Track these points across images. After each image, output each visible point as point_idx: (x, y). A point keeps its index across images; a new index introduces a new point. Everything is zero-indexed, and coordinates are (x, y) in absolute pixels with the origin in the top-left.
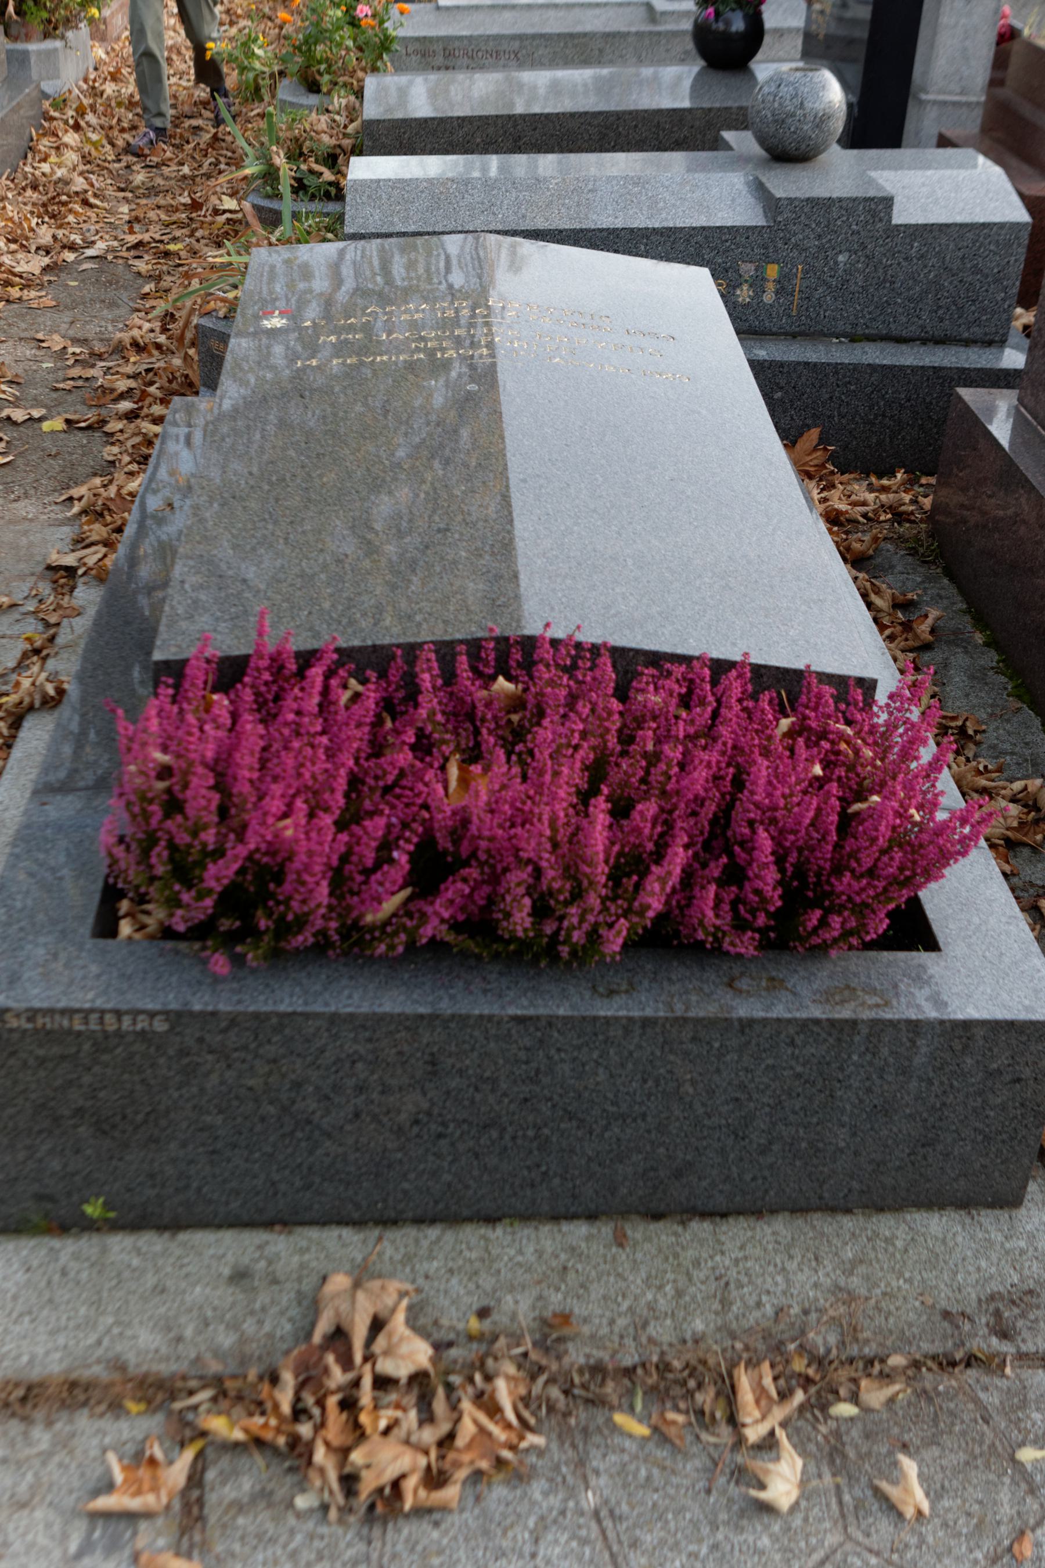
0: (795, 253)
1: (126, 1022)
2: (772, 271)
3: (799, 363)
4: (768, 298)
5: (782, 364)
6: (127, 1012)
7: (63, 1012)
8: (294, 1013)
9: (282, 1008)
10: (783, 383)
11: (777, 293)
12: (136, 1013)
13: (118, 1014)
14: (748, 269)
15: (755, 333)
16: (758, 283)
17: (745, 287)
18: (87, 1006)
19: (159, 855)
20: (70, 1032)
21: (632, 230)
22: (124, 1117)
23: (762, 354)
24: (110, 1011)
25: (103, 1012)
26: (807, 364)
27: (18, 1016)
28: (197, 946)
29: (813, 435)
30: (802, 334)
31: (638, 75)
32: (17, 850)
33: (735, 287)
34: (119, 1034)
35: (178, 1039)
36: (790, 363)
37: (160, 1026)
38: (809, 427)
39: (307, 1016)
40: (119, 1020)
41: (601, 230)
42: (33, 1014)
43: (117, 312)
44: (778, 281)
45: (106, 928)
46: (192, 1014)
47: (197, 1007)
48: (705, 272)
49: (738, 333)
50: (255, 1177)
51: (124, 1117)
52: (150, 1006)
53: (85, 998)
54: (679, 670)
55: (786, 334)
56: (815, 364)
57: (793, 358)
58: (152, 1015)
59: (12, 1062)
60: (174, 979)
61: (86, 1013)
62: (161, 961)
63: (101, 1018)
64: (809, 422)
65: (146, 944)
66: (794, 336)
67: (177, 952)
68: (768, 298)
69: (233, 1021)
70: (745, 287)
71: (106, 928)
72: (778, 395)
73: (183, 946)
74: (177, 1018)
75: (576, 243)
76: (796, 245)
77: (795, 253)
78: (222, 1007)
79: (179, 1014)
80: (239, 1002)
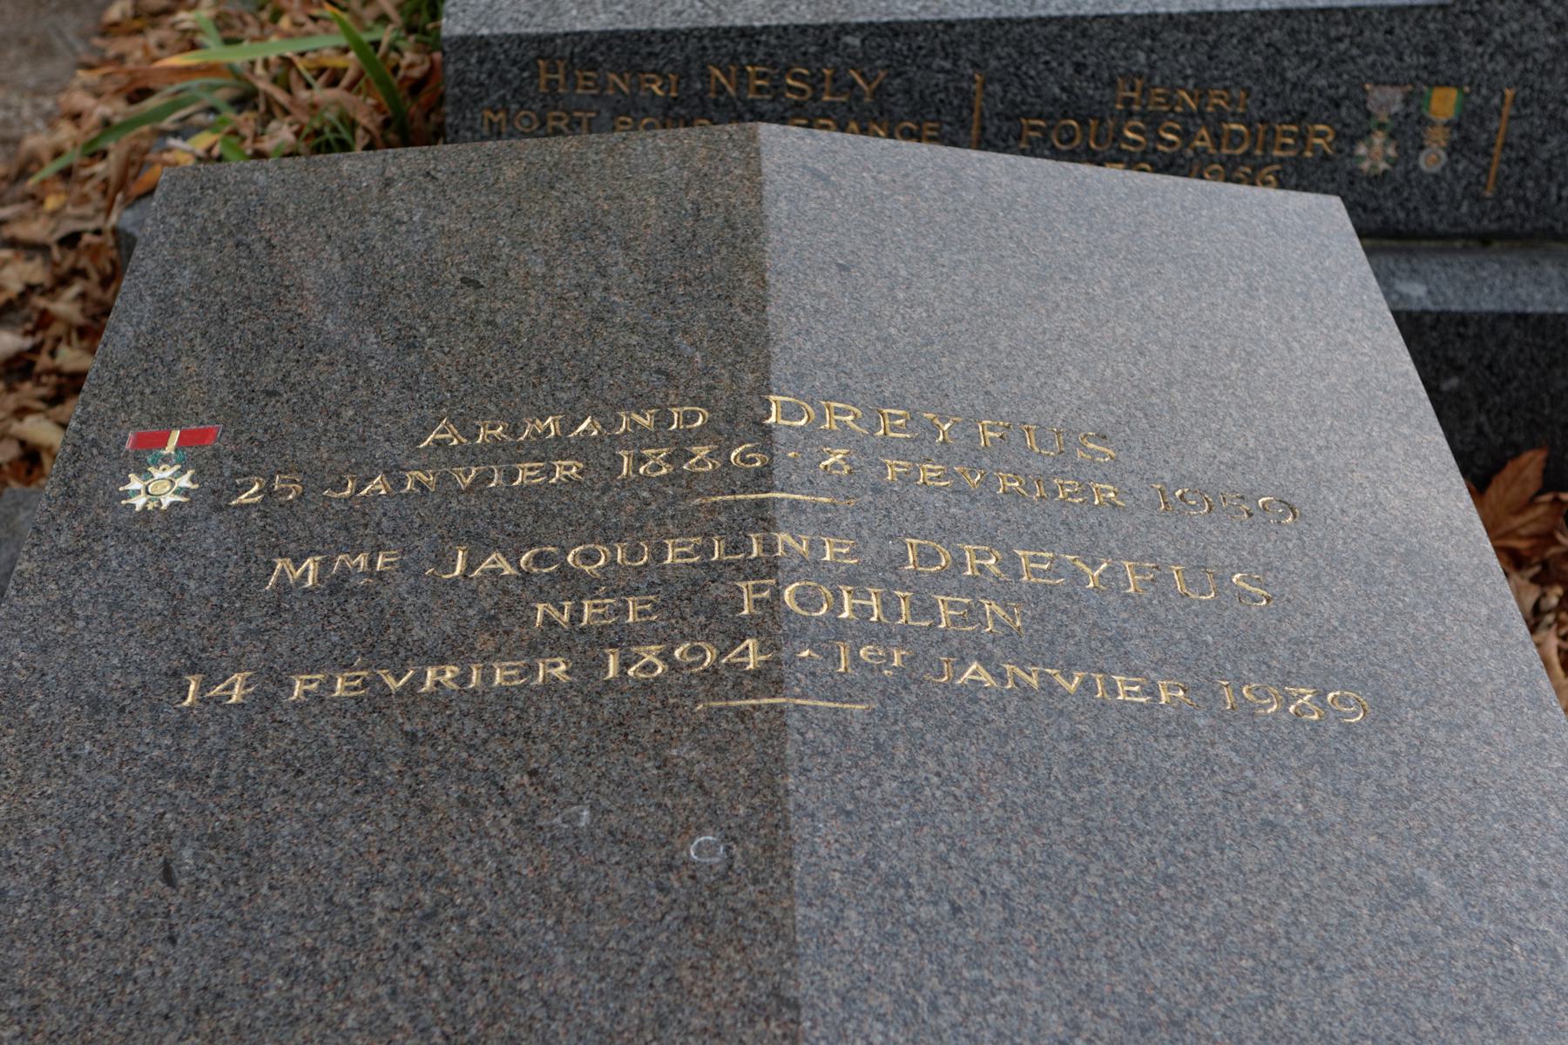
0: (1501, 63)
2: (1444, 104)
3: (1503, 316)
4: (1432, 160)
5: (1462, 319)
10: (1462, 357)
11: (1452, 149)
14: (1386, 100)
15: (1397, 235)
16: (1408, 130)
17: (1378, 139)
21: (1117, 20)
23: (1416, 292)
26: (1522, 317)
29: (1531, 464)
30: (1507, 236)
33: (1353, 140)
36: (1481, 317)
38: (1518, 450)
41: (1044, 21)
43: (48, 68)
44: (1455, 125)
48: (1336, 201)
49: (1362, 234)
54: (1023, 145)
55: (1467, 236)
56: (1542, 318)
57: (1488, 303)
64: (1519, 437)
66: (1485, 240)
68: (1432, 160)
70: (1378, 139)
72: (1453, 382)
75: (1003, 132)
76: (1503, 46)
77: (1501, 63)
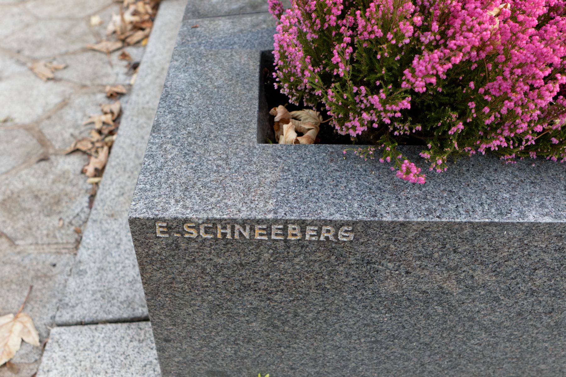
1: (310, 232)
6: (312, 223)
7: (244, 223)
8: (491, 224)
9: (477, 218)
12: (321, 224)
13: (303, 225)
18: (270, 216)
19: (342, 53)
20: (251, 241)
22: (296, 315)
24: (294, 222)
25: (286, 223)
27: (197, 227)
28: (371, 150)
31: (188, 22)
32: (176, 64)
34: (301, 244)
35: (362, 248)
37: (345, 236)
39: (502, 226)
40: (303, 232)
42: (212, 225)
45: (269, 133)
46: (381, 224)
47: (388, 218)
50: (409, 359)
51: (296, 315)
52: (337, 217)
53: (264, 209)
58: (338, 225)
59: (189, 269)
60: (353, 185)
61: (268, 224)
62: (333, 166)
63: (285, 229)
65: (313, 147)
67: (347, 157)
69: (424, 230)
71: (269, 133)
73: (357, 151)
74: (362, 229)
78: (412, 217)
79: (367, 225)
80: (429, 211)
